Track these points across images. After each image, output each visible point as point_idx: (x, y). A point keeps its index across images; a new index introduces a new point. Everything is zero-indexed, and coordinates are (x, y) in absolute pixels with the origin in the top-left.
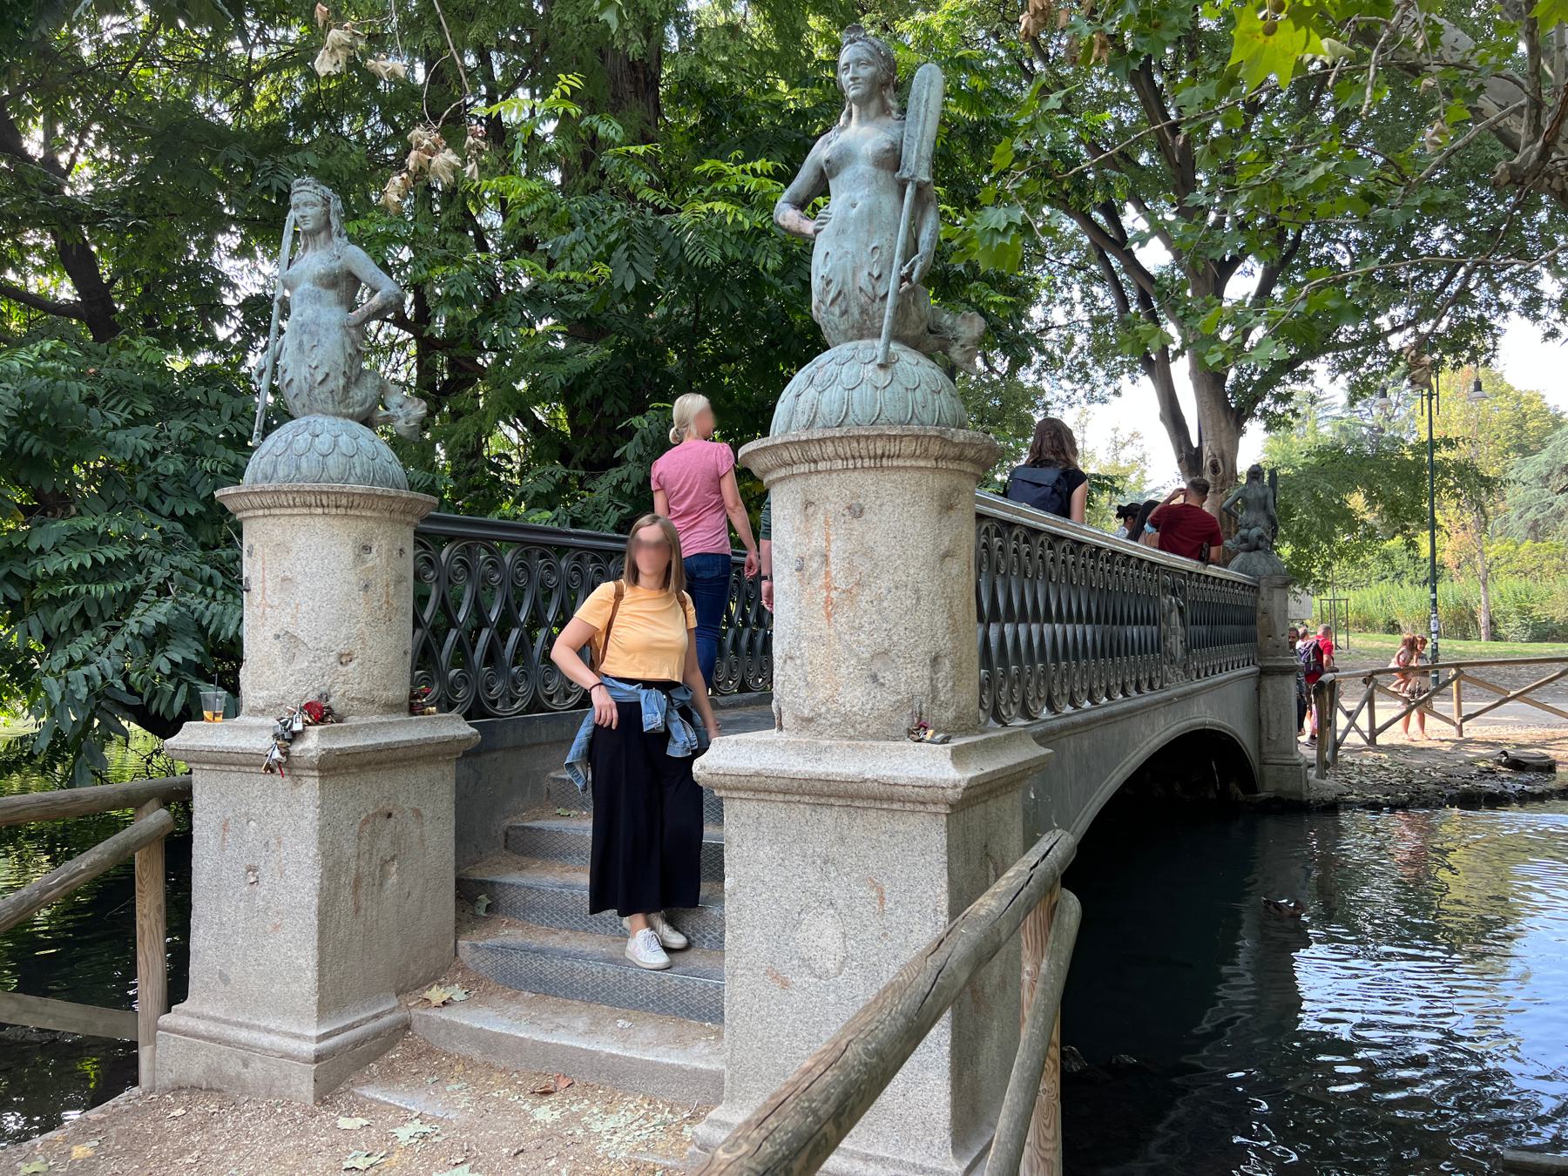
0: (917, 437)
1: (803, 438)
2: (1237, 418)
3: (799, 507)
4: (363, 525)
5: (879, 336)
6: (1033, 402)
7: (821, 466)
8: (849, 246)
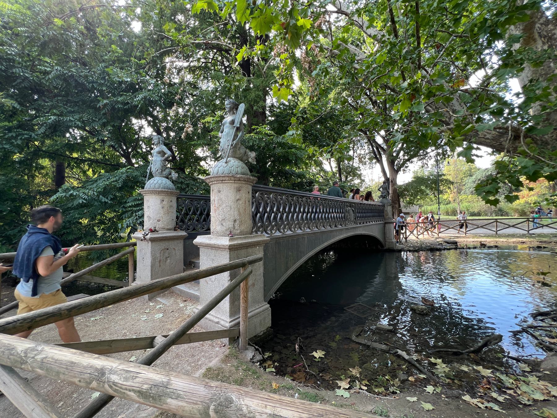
2: (397, 171)
4: (162, 196)
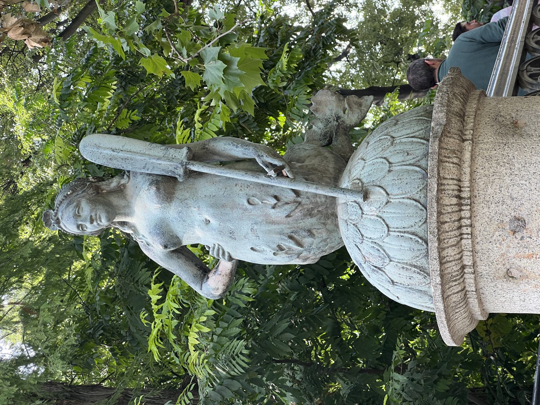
0: (440, 162)
1: (438, 280)
3: (511, 284)
5: (334, 198)
6: (379, 11)
7: (467, 261)
8: (245, 227)
